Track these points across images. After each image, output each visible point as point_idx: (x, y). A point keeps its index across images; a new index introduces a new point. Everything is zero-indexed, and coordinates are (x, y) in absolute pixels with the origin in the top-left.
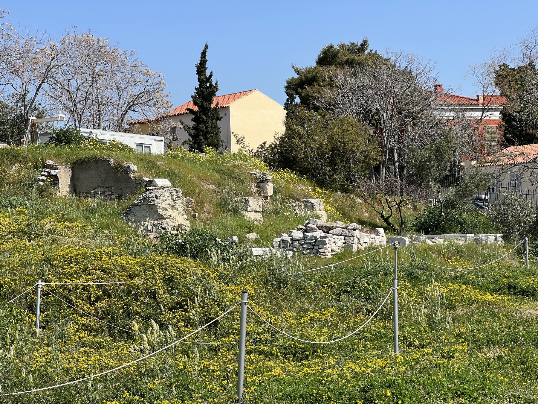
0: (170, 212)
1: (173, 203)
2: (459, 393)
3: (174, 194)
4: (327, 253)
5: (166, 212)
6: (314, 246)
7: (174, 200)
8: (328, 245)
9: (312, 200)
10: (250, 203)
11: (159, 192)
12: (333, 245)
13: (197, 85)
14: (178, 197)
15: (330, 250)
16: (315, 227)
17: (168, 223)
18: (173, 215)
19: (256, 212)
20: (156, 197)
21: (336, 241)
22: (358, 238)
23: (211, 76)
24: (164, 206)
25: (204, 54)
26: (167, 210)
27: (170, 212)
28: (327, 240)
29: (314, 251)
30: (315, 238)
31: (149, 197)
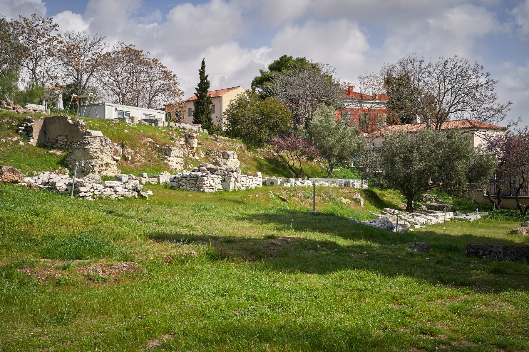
0: (99, 154)
1: (102, 148)
2: (356, 294)
3: (104, 142)
4: (205, 188)
5: (95, 154)
6: (196, 182)
7: (103, 146)
8: (206, 182)
9: (228, 152)
10: (172, 151)
11: (90, 140)
12: (212, 182)
13: (199, 81)
14: (107, 144)
15: (208, 185)
16: (205, 168)
17: (96, 162)
18: (101, 156)
19: (178, 157)
20: (89, 143)
21: (214, 179)
22: (234, 177)
23: (207, 76)
24: (94, 150)
25: (203, 63)
26: (96, 153)
27: (99, 154)
28: (205, 178)
29: (197, 185)
30: (198, 176)
31: (84, 143)
